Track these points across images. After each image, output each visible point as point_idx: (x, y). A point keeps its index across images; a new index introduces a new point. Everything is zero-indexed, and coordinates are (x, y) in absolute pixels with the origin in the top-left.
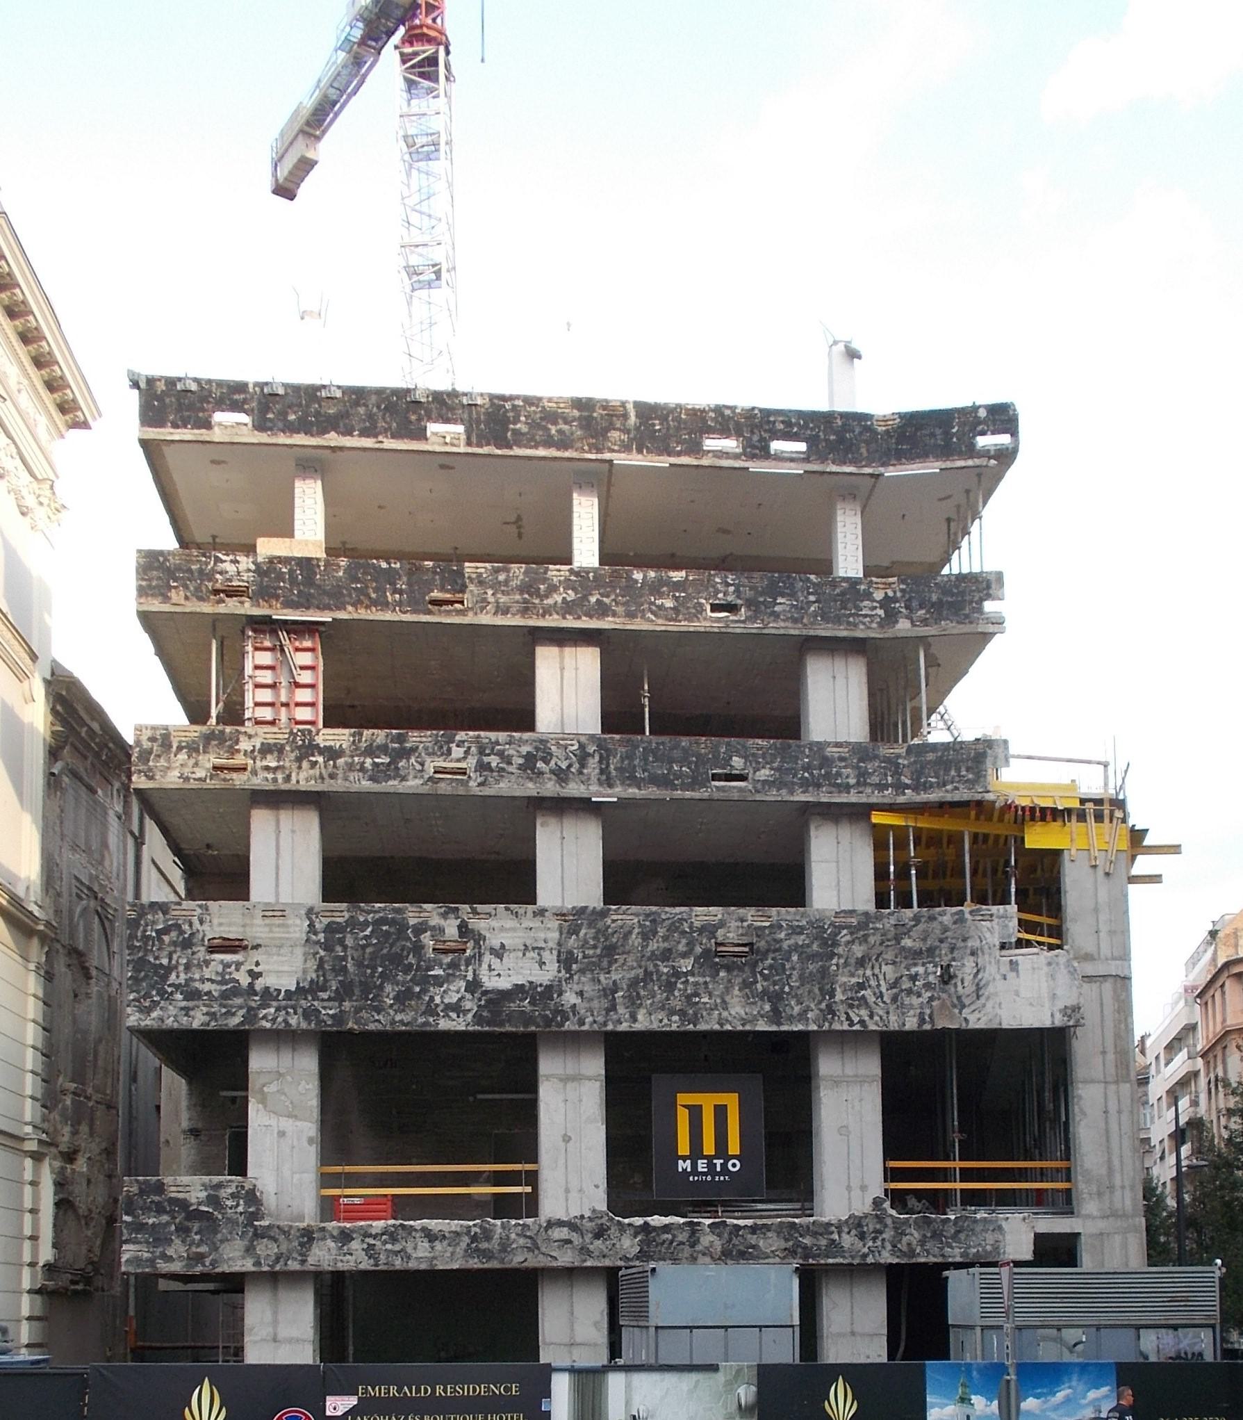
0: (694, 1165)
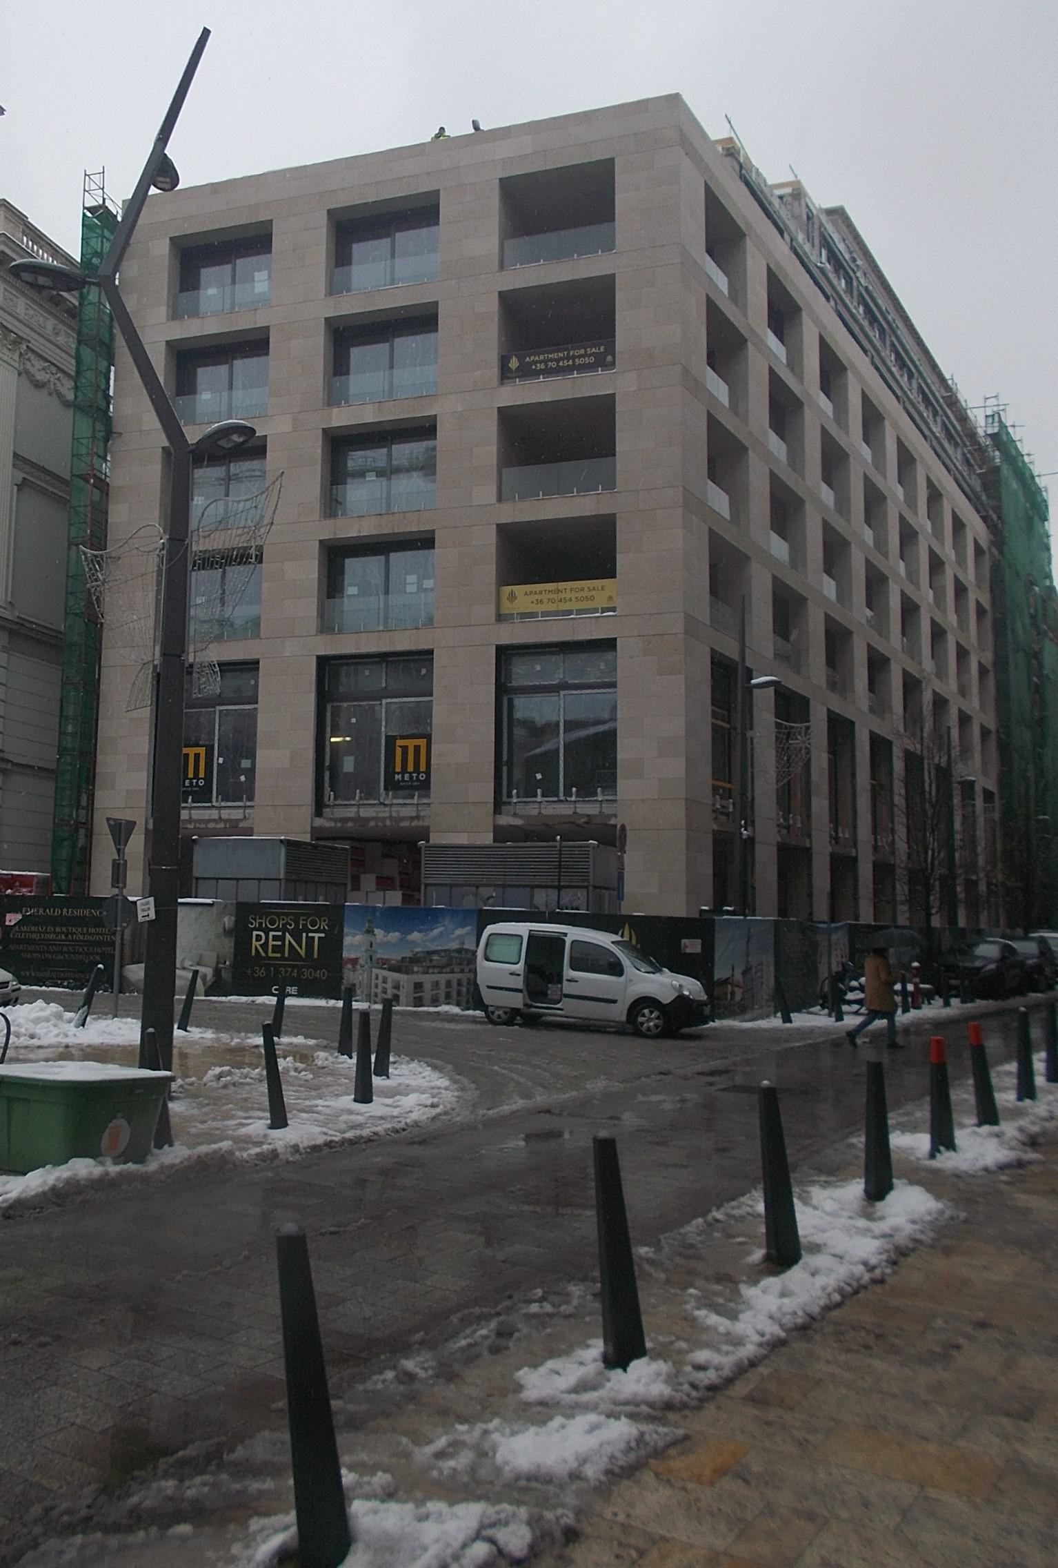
0: (403, 777)
